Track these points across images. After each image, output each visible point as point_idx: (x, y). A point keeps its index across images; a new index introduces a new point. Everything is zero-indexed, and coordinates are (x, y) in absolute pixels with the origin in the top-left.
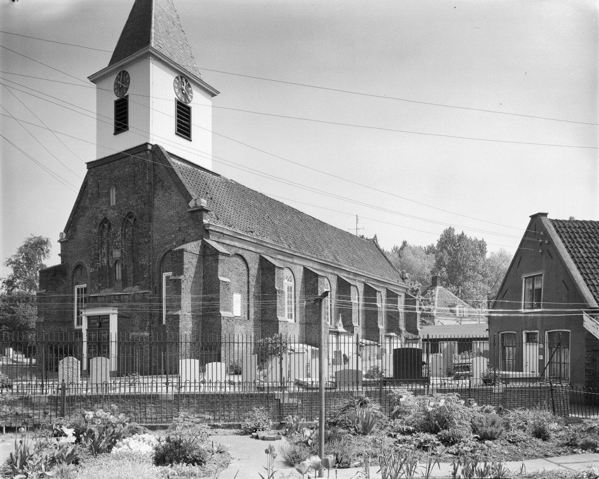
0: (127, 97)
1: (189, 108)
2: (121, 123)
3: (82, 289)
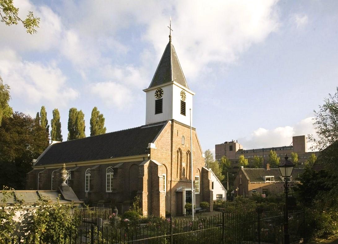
1: (185, 103)
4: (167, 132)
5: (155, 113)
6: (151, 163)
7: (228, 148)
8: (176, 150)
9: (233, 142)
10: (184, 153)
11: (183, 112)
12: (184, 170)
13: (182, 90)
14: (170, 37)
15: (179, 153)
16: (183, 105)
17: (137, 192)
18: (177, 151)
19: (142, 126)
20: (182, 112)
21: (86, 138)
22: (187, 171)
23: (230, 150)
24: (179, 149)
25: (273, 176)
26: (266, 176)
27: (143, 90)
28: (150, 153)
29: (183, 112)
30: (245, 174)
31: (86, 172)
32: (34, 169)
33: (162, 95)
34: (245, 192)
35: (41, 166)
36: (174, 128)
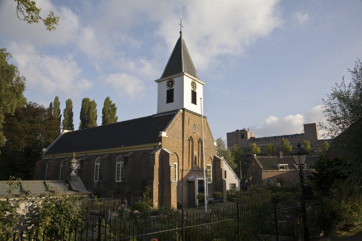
0: (173, 89)
1: (196, 92)
4: (178, 121)
6: (163, 151)
8: (188, 139)
9: (244, 130)
10: (196, 142)
11: (194, 101)
12: (196, 158)
13: (193, 80)
14: (181, 32)
15: (191, 142)
16: (194, 94)
18: (189, 139)
20: (192, 101)
22: (199, 159)
24: (191, 137)
25: (287, 165)
26: (280, 165)
27: (155, 81)
28: (161, 142)
29: (194, 101)
30: (258, 162)
31: (96, 161)
32: (43, 158)
33: (173, 85)
36: (186, 117)
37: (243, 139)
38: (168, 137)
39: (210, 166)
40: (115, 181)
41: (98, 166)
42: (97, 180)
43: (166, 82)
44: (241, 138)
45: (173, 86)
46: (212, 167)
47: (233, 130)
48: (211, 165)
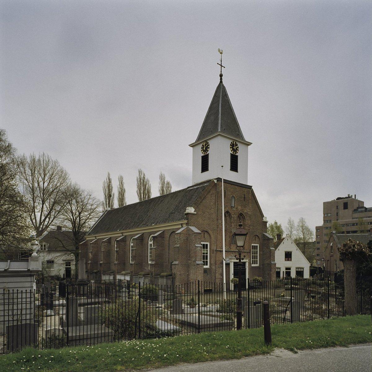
0: (208, 155)
1: (237, 156)
2: (205, 167)
3: (255, 264)
5: (201, 172)
7: (341, 206)
13: (232, 141)
14: (221, 76)
17: (173, 264)
19: (188, 187)
21: (172, 193)
23: (347, 203)
31: (149, 240)
32: (87, 239)
34: (336, 265)
35: (154, 226)
37: (346, 210)
38: (196, 213)
39: (257, 246)
40: (148, 263)
41: (151, 244)
42: (257, 264)
43: (201, 146)
44: (343, 208)
45: (208, 151)
46: (259, 247)
47: (332, 197)
48: (258, 245)
